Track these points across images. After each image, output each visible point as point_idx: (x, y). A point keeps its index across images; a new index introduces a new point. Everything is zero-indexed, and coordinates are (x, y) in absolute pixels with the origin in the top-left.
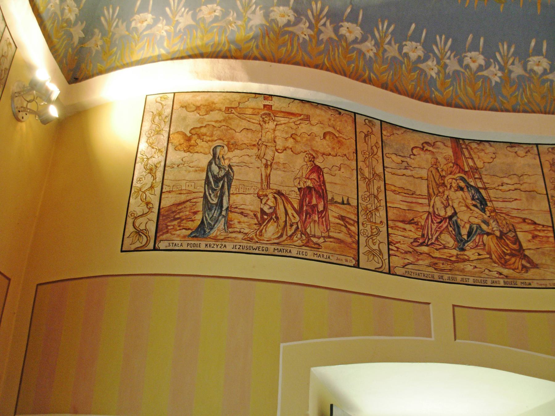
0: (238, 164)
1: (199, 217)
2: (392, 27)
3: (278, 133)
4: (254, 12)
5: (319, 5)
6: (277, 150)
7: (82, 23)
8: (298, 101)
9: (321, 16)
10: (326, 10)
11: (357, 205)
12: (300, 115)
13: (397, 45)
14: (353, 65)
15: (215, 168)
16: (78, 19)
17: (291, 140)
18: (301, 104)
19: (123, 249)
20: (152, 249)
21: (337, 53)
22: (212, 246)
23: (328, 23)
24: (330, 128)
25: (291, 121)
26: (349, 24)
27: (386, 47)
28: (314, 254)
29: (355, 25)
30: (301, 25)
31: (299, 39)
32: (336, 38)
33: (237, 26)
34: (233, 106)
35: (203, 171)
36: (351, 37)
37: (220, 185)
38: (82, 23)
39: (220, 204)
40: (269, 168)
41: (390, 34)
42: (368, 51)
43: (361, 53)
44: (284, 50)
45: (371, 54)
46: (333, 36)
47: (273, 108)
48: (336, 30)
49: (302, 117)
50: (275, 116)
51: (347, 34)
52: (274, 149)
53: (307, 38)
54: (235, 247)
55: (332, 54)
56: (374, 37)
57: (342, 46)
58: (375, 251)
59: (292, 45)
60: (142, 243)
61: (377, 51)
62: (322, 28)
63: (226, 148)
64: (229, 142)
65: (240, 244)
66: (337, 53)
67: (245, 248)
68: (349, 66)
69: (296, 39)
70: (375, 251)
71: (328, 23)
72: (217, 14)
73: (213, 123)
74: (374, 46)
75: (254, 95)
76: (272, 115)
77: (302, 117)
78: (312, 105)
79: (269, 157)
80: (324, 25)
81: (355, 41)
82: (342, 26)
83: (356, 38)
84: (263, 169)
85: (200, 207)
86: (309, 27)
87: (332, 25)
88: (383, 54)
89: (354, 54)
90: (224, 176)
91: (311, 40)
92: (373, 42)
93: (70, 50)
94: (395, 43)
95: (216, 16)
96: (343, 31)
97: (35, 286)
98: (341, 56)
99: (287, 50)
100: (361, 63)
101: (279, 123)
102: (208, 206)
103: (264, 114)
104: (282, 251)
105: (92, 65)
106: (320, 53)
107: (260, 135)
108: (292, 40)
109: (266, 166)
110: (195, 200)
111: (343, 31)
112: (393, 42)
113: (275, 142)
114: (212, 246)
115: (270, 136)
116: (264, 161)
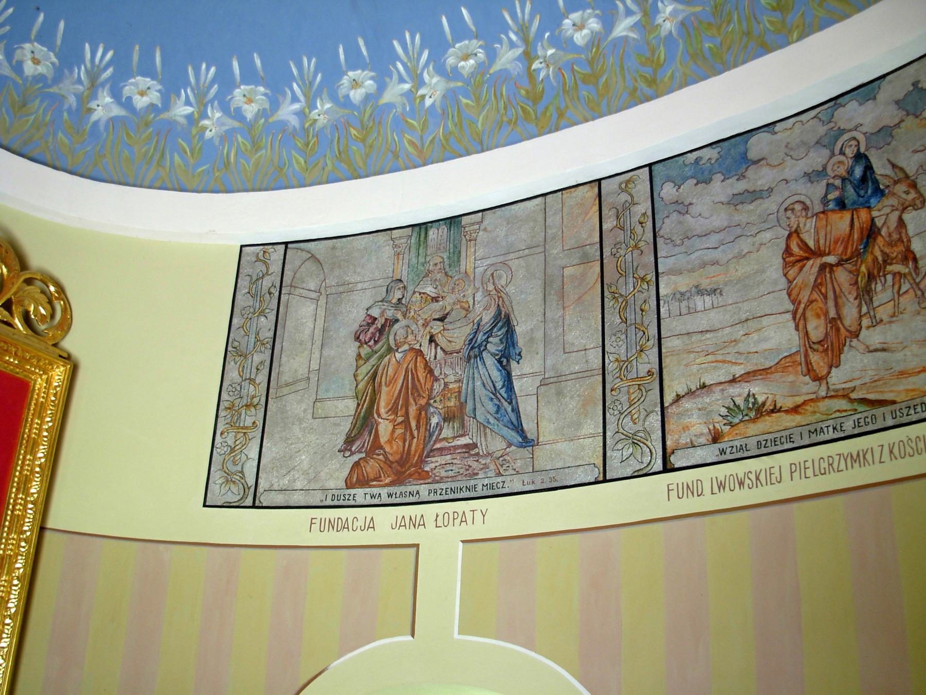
11: (288, 250)
19: (413, 550)
20: (662, 469)
22: (735, 448)
24: (308, 249)
28: (810, 431)
54: (475, 488)
58: (635, 437)
60: (642, 463)
65: (731, 444)
67: (342, 498)
70: (635, 437)
97: (789, 465)
104: (469, 521)
110: (858, 460)
114: (735, 448)
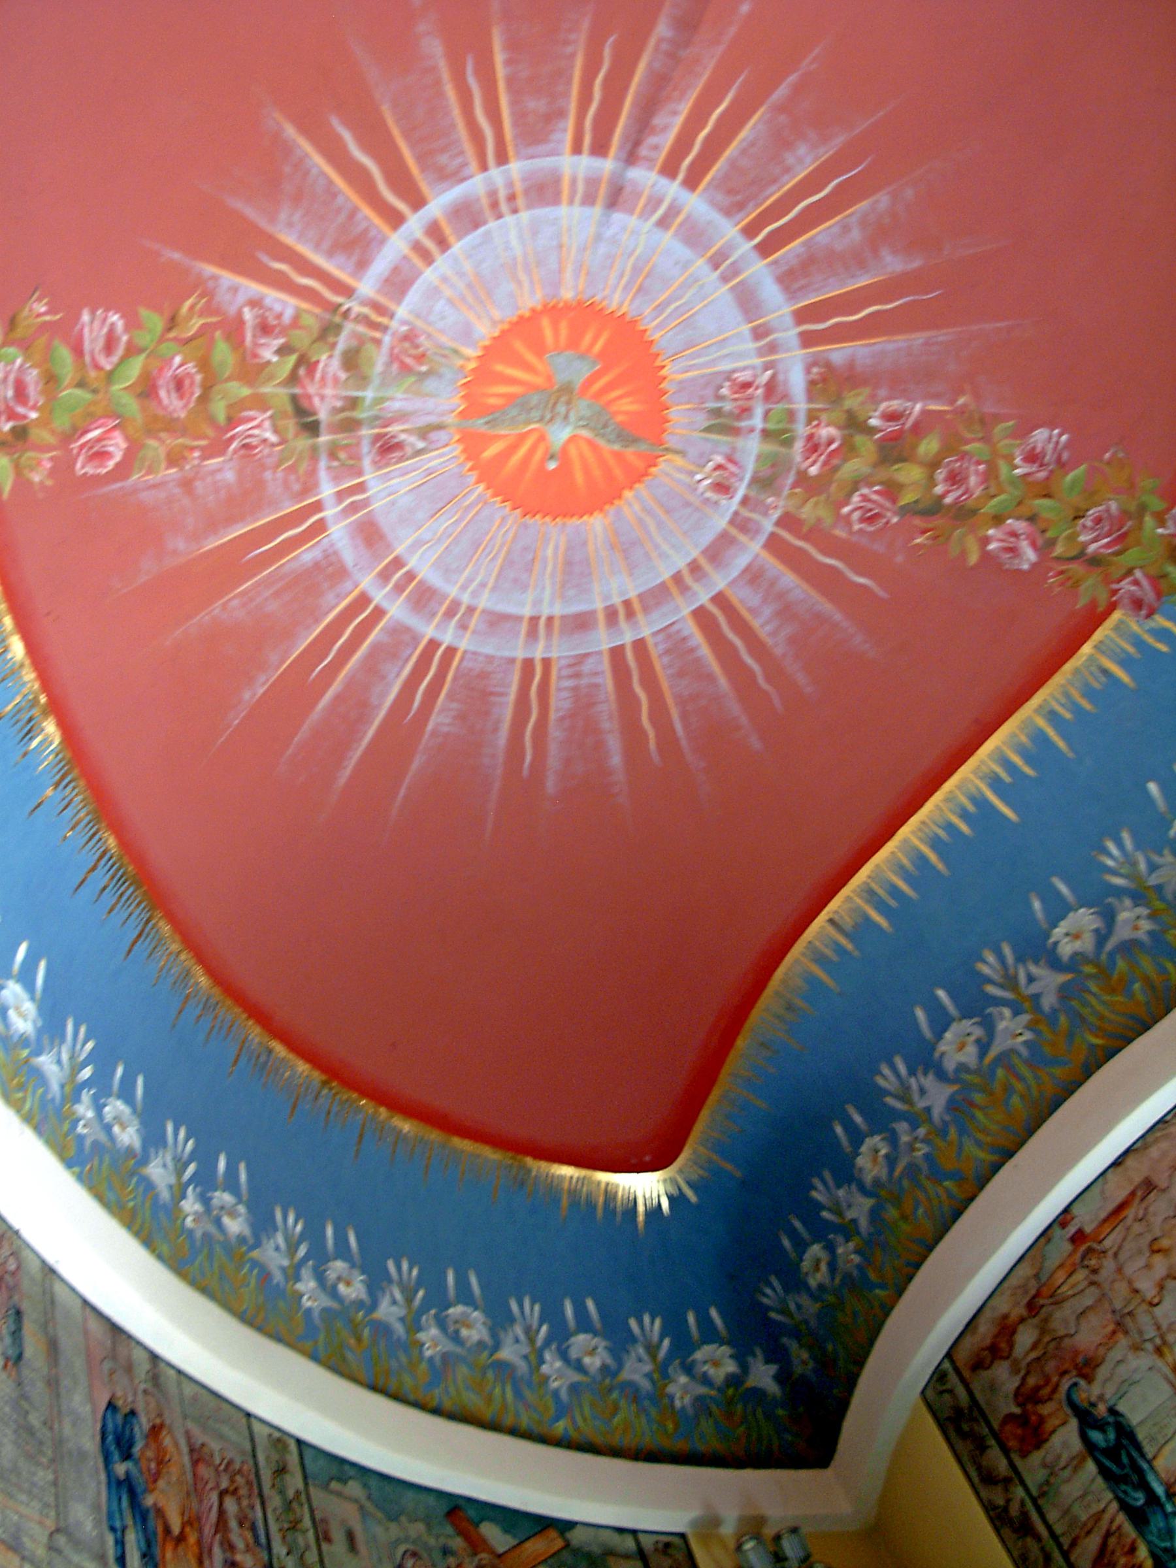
0: (1119, 1395)
1: (1143, 1552)
2: (1126, 836)
3: (1129, 1270)
4: (922, 1091)
5: (991, 958)
6: (1152, 1305)
7: (754, 1355)
8: (1110, 1170)
9: (1011, 971)
10: (1007, 950)
12: (1133, 1194)
13: (1166, 852)
14: (1137, 986)
15: (1096, 1436)
16: (741, 1358)
17: (1158, 1259)
18: (1120, 1169)
21: (1094, 1001)
23: (1033, 969)
25: (1129, 1221)
26: (1063, 923)
27: (1153, 880)
29: (1071, 915)
30: (1001, 1025)
31: (1019, 1054)
32: (1069, 976)
33: (923, 1141)
34: (1033, 1292)
35: (1083, 1460)
36: (1086, 944)
37: (1125, 1460)
38: (754, 1355)
39: (1152, 1498)
40: (1166, 1350)
41: (1136, 851)
42: (1136, 928)
43: (1129, 947)
44: (1015, 1100)
45: (1146, 925)
46: (1062, 978)
47: (1088, 1229)
48: (1055, 964)
49: (1139, 1193)
50: (1100, 1242)
51: (1078, 945)
52: (1145, 1307)
53: (1028, 1036)
55: (1085, 1011)
56: (1119, 892)
57: (1090, 976)
59: (1020, 1077)
61: (1148, 908)
62: (1033, 989)
63: (1082, 1383)
64: (1076, 1366)
66: (1094, 1001)
68: (1131, 995)
69: (1016, 1060)
71: (1033, 969)
72: (883, 1152)
73: (1033, 1355)
74: (1136, 905)
75: (1042, 1240)
76: (1095, 1245)
77: (1139, 1193)
78: (1136, 1150)
79: (1151, 1333)
80: (1031, 979)
81: (1101, 938)
82: (1056, 944)
83: (1096, 931)
84: (1159, 1363)
85: (1130, 1530)
86: (1016, 1013)
87: (1042, 963)
88: (1162, 899)
89: (1121, 965)
90: (1118, 1439)
91: (1038, 1033)
92: (1128, 902)
93: (780, 1412)
94: (1161, 855)
95: (887, 1156)
96: (1066, 949)
98: (1106, 998)
99: (1022, 1097)
100: (1146, 964)
101: (1115, 1249)
102: (1139, 1518)
103: (1083, 1258)
105: (958, 523)
106: (1070, 1035)
107: (1106, 1305)
108: (1011, 1069)
109: (1159, 1351)
111: (1066, 949)
112: (1156, 859)
113: (1137, 1291)
115: (1122, 1288)
116: (1149, 1346)
